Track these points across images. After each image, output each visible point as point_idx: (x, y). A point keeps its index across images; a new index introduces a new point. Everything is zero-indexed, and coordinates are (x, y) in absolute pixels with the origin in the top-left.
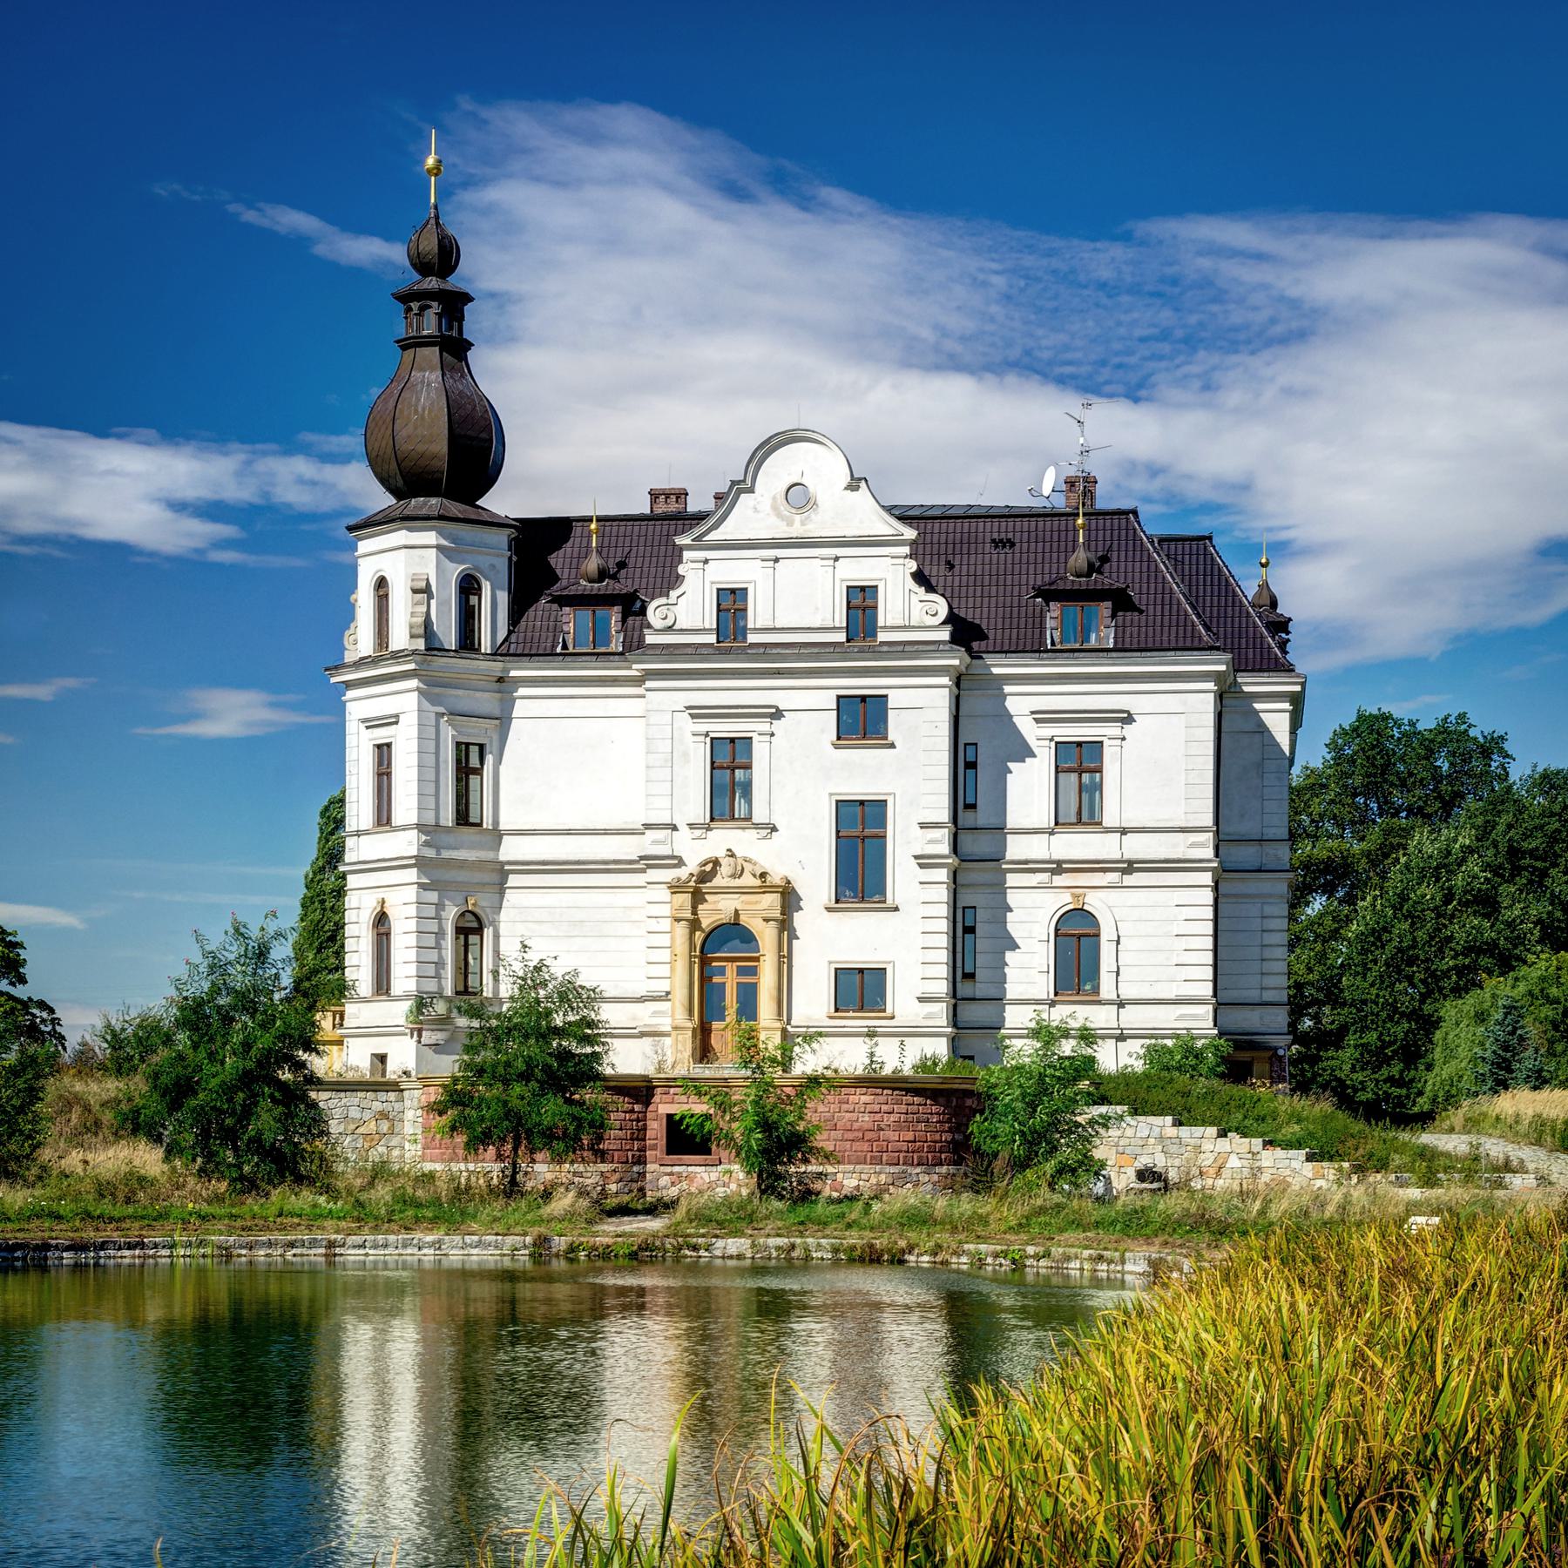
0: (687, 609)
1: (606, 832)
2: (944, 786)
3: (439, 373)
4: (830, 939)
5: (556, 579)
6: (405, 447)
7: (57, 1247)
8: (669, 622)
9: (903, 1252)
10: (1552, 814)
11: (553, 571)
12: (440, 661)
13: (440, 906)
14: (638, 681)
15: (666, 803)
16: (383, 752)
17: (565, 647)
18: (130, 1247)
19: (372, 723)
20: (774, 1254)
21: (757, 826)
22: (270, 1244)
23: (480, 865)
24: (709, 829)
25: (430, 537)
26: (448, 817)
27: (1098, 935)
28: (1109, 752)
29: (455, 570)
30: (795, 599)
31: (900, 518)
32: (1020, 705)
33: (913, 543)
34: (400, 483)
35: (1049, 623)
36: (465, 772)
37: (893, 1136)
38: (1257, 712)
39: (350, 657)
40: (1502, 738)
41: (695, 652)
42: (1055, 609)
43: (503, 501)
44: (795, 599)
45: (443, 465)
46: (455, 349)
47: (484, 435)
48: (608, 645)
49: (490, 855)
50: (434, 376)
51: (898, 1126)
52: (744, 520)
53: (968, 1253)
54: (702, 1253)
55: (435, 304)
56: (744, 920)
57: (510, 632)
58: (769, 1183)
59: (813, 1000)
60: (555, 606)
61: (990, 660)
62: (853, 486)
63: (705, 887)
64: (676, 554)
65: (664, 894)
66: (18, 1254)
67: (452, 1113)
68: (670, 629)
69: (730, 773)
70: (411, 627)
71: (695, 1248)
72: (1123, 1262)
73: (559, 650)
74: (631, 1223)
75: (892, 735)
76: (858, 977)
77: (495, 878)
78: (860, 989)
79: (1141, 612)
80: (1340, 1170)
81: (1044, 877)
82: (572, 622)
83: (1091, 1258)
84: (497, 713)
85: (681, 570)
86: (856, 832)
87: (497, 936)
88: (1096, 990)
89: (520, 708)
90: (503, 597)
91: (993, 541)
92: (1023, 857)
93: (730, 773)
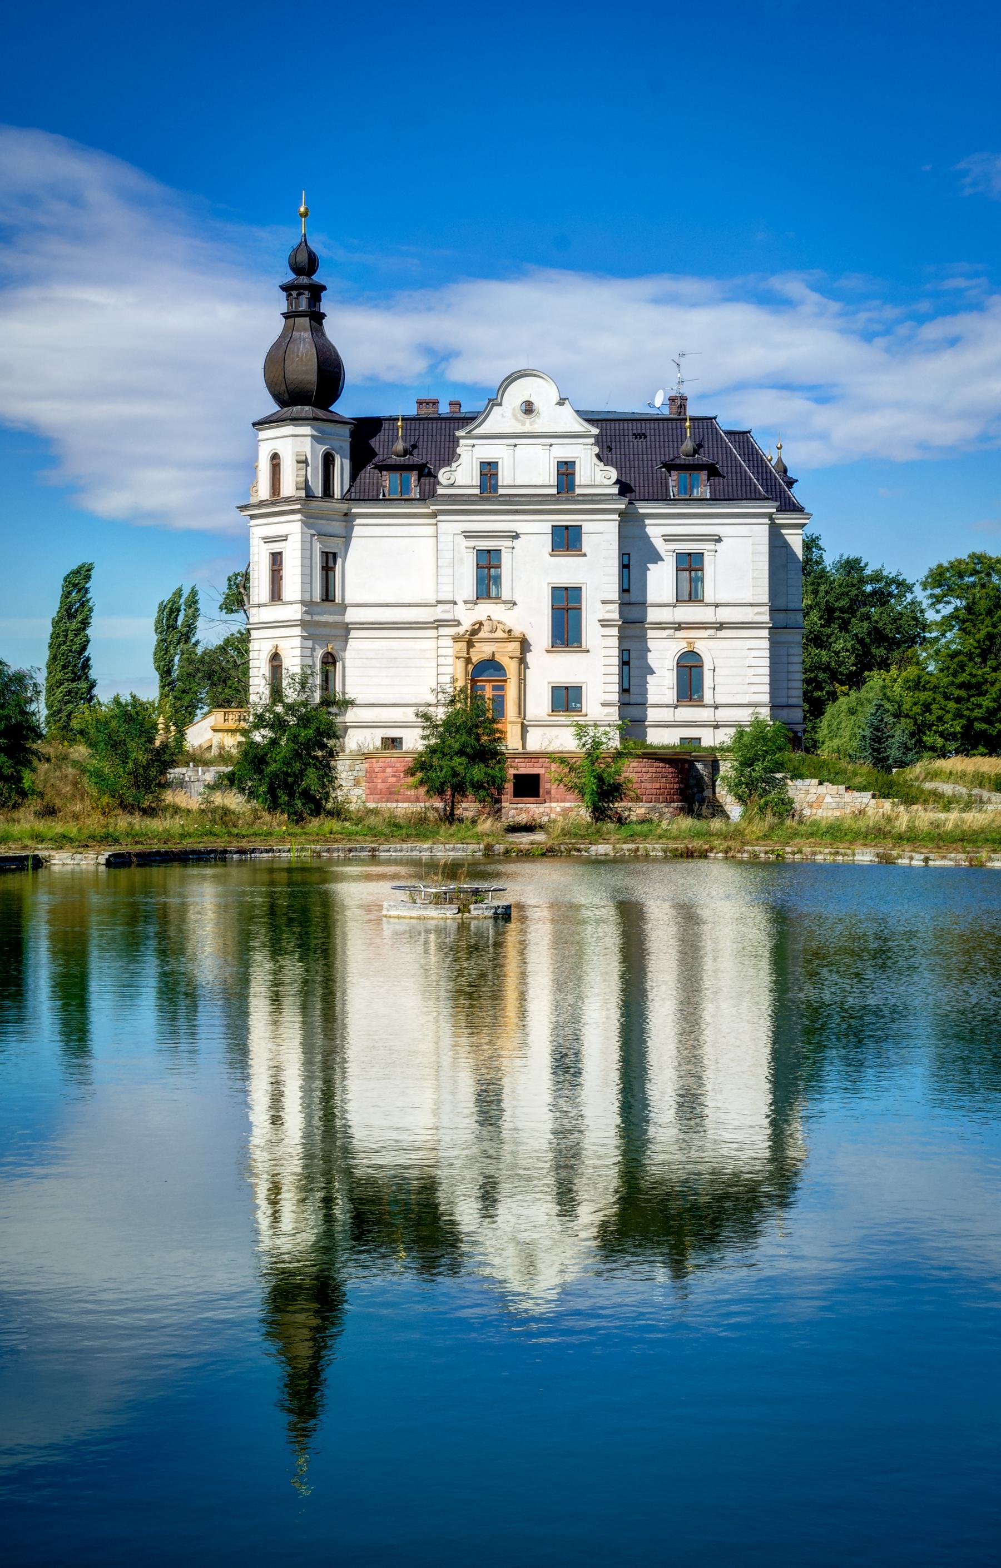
0: (461, 475)
1: (409, 605)
2: (615, 579)
3: (310, 333)
4: (548, 669)
5: (375, 455)
6: (290, 376)
7: (231, 852)
8: (451, 481)
9: (707, 851)
10: (853, 585)
11: (373, 450)
12: (314, 504)
13: (313, 649)
14: (434, 515)
15: (450, 588)
16: (276, 559)
17: (384, 495)
18: (267, 851)
19: (268, 540)
20: (627, 854)
21: (505, 602)
22: (338, 850)
23: (335, 625)
24: (476, 604)
25: (307, 430)
26: (317, 596)
27: (702, 666)
28: (707, 560)
29: (322, 449)
30: (529, 468)
31: (587, 420)
32: (655, 531)
33: (596, 437)
34: (286, 397)
35: (671, 483)
36: (328, 569)
37: (649, 786)
38: (783, 535)
39: (254, 500)
40: (817, 538)
41: (468, 499)
42: (675, 474)
43: (346, 407)
44: (529, 468)
45: (314, 388)
46: (317, 318)
47: (337, 370)
48: (408, 493)
49: (337, 618)
50: (307, 335)
51: (652, 780)
52: (498, 420)
53: (748, 852)
54: (583, 853)
55: (306, 292)
56: (497, 658)
57: (351, 486)
58: (599, 813)
59: (539, 703)
60: (376, 471)
61: (638, 504)
62: (561, 402)
63: (475, 638)
64: (455, 442)
65: (449, 642)
66: (212, 856)
67: (420, 775)
68: (452, 485)
69: (488, 570)
70: (297, 483)
71: (579, 850)
72: (854, 855)
73: (381, 497)
74: (523, 837)
75: (584, 550)
76: (564, 691)
77: (342, 632)
78: (566, 699)
79: (724, 477)
80: (893, 803)
81: (670, 632)
82: (388, 479)
83: (830, 853)
84: (343, 534)
85: (459, 450)
86: (563, 605)
87: (344, 668)
88: (701, 698)
89: (357, 531)
90: (347, 463)
91: (634, 434)
92: (658, 621)
93: (488, 570)
